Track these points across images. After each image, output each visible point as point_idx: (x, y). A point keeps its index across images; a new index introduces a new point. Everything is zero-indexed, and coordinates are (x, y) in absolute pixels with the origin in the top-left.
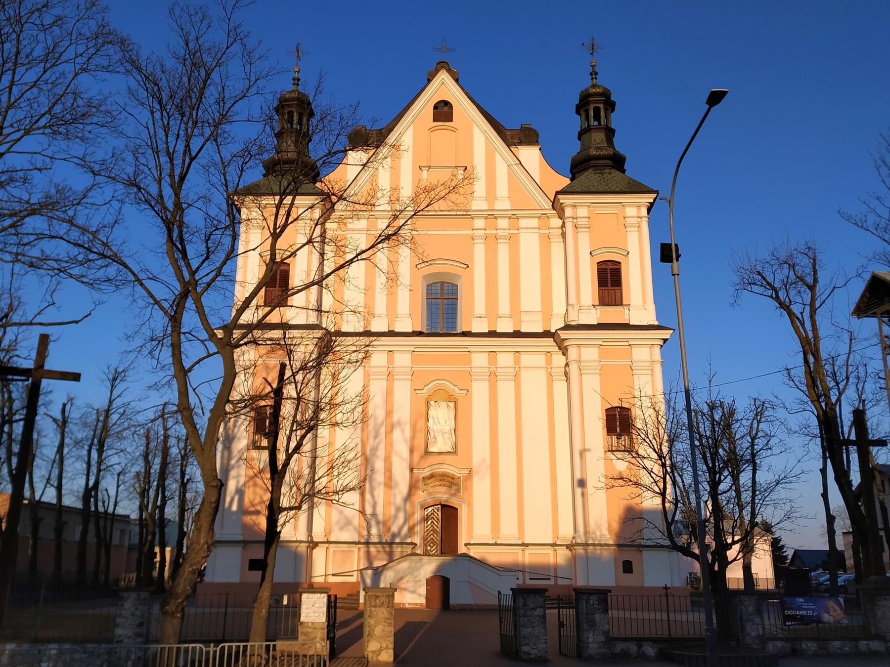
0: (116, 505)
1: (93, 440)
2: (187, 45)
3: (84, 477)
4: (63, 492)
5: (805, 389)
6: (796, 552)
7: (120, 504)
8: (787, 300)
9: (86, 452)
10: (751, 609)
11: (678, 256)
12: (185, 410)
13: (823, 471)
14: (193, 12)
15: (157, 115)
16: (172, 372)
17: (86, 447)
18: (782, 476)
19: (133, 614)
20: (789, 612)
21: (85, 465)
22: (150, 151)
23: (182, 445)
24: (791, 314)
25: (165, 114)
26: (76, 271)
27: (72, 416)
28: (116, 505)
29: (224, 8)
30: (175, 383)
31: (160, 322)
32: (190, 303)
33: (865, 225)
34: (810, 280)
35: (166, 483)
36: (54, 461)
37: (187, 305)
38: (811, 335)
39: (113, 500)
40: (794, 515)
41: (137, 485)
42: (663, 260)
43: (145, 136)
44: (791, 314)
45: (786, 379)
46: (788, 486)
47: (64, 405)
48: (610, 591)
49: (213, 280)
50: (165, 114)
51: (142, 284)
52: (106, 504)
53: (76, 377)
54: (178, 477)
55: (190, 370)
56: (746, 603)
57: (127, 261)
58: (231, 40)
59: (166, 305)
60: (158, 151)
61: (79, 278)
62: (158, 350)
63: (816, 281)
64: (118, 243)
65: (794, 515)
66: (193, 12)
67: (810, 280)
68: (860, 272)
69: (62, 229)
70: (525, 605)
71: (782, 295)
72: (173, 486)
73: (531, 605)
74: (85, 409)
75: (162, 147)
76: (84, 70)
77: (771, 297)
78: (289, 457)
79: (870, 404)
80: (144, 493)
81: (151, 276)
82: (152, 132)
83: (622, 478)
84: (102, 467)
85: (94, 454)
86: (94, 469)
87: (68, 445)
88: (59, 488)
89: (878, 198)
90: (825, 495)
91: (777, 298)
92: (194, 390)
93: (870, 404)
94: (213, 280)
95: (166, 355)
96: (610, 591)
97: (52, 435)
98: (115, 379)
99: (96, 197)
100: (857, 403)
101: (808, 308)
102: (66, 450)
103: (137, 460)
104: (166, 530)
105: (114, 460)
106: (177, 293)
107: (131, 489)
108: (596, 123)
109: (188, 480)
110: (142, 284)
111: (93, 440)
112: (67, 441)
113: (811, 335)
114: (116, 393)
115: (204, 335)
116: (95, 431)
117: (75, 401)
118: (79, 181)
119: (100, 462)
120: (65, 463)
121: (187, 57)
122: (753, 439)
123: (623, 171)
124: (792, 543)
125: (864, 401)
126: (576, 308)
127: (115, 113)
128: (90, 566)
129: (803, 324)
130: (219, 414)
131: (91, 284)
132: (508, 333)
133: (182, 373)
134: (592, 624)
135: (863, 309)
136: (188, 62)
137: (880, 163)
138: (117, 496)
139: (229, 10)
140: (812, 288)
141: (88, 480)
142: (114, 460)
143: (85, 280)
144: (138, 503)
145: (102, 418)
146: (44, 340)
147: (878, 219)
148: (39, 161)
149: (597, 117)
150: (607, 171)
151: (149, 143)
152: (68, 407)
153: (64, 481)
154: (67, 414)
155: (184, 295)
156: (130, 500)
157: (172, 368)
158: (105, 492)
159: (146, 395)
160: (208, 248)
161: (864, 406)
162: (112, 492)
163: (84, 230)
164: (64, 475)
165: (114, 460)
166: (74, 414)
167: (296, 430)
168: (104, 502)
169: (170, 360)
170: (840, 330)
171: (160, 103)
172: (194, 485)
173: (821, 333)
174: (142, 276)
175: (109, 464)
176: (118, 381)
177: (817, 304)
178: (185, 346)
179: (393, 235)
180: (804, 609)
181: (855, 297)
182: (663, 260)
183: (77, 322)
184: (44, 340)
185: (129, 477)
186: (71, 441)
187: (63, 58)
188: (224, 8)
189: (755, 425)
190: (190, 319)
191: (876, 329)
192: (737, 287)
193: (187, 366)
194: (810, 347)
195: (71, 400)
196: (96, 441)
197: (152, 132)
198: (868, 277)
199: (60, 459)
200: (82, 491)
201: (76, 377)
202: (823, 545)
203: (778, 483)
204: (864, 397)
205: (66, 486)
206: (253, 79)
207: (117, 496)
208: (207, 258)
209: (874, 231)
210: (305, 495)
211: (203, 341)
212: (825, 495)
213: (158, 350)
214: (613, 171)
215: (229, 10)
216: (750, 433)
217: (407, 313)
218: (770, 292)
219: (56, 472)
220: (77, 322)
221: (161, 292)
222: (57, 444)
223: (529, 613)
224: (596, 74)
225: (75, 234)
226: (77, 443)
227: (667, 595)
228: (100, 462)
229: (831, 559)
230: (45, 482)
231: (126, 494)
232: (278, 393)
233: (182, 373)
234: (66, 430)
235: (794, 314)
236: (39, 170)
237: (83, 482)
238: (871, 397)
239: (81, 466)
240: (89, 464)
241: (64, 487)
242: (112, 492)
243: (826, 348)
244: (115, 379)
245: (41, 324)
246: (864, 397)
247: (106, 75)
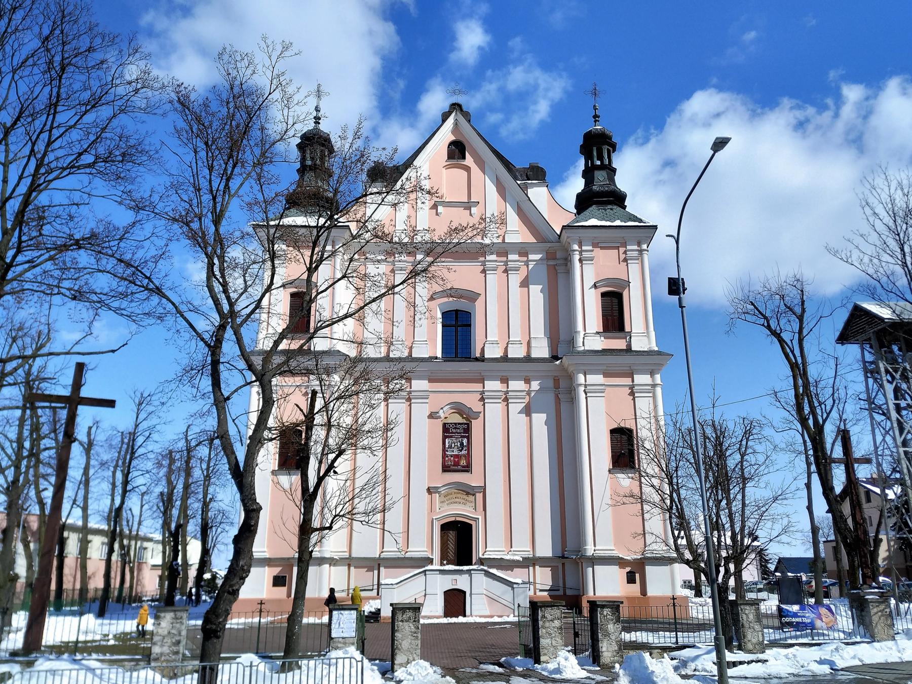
0: (140, 523)
1: (117, 461)
2: (232, 88)
3: (110, 497)
4: (89, 512)
5: (794, 413)
6: (781, 561)
7: (144, 523)
8: (778, 328)
9: (111, 474)
10: (751, 617)
11: (684, 290)
12: (222, 436)
13: (808, 486)
14: (239, 58)
15: (203, 154)
16: (212, 400)
17: (112, 469)
18: (780, 493)
19: (169, 633)
20: (787, 620)
21: (110, 487)
22: (192, 189)
23: (204, 466)
24: (781, 341)
25: (210, 154)
26: (116, 304)
27: (98, 438)
28: (140, 523)
29: (270, 57)
30: (214, 410)
31: (201, 352)
32: (229, 333)
33: (850, 260)
34: (798, 310)
35: (189, 502)
36: (80, 483)
37: (226, 336)
38: (799, 360)
39: (137, 519)
40: (791, 529)
41: (161, 504)
42: (114, 407)
43: (189, 174)
44: (781, 341)
45: (773, 400)
46: (785, 502)
47: (90, 428)
48: (622, 603)
49: (253, 312)
50: (210, 154)
51: (182, 316)
52: (130, 524)
53: (111, 404)
54: (201, 496)
55: (228, 398)
56: (747, 612)
57: (169, 293)
58: (274, 87)
59: (207, 336)
60: (199, 190)
61: (117, 311)
62: (198, 379)
63: (803, 310)
64: (160, 276)
65: (791, 529)
66: (239, 58)
67: (798, 310)
68: (844, 302)
69: (110, 264)
70: (544, 617)
71: (773, 325)
72: (195, 505)
73: (549, 617)
74: (110, 432)
75: (204, 184)
76: (122, 111)
77: (763, 325)
78: (320, 480)
79: (851, 423)
80: (166, 514)
81: (192, 308)
82: (195, 170)
83: (632, 496)
84: (129, 488)
85: (119, 475)
86: (119, 490)
87: (94, 467)
88: (85, 509)
89: (861, 236)
90: (810, 508)
91: (769, 327)
92: (234, 421)
93: (851, 423)
94: (253, 312)
95: (206, 383)
96: (622, 603)
97: (79, 457)
98: (140, 404)
99: (139, 234)
100: (838, 423)
101: (797, 335)
102: (91, 472)
103: (159, 480)
104: (188, 548)
105: (140, 481)
106: (217, 324)
107: (155, 508)
108: (598, 163)
109: (211, 499)
110: (182, 316)
111: (117, 461)
112: (92, 462)
113: (799, 360)
114: (142, 416)
115: (242, 365)
116: (119, 453)
117: (100, 425)
118: (122, 217)
119: (126, 482)
120: (91, 484)
121: (231, 99)
122: (742, 456)
123: (624, 207)
124: (776, 551)
125: (845, 420)
126: (582, 333)
127: (151, 153)
128: (115, 583)
129: (792, 352)
130: (256, 442)
131: (129, 317)
132: (519, 359)
133: (220, 402)
134: (607, 635)
135: (843, 338)
136: (231, 105)
137: (864, 203)
138: (141, 516)
139: (274, 59)
140: (801, 318)
141: (113, 500)
142: (139, 480)
143: (124, 312)
144: (161, 521)
145: (126, 441)
146: (80, 368)
147: (861, 255)
148: (76, 197)
149: (600, 158)
150: (609, 207)
151: (192, 181)
152: (93, 430)
153: (90, 501)
154: (92, 437)
155: (222, 328)
156: (153, 519)
157: (212, 396)
158: (129, 512)
159: (180, 418)
160: (245, 281)
161: (845, 425)
162: (136, 511)
163: (128, 265)
164: (90, 496)
165: (140, 481)
166: (100, 437)
167: (327, 454)
168: (128, 522)
169: (210, 389)
170: (826, 356)
171: (206, 144)
172: (215, 504)
173: (810, 358)
174: (183, 308)
175: (135, 485)
176: (144, 405)
177: (805, 332)
178: (224, 374)
179: (423, 271)
180: (799, 617)
181: (840, 326)
182: (114, 407)
183: (113, 351)
184: (80, 368)
185: (153, 498)
186: (96, 463)
187: (103, 101)
188: (270, 57)
189: (744, 443)
190: (229, 348)
191: (859, 356)
192: (732, 316)
193: (226, 394)
194: (799, 370)
195: (97, 423)
196: (120, 463)
197: (195, 170)
198: (850, 307)
199: (86, 482)
200: (107, 510)
201: (111, 404)
202: (810, 554)
203: (775, 499)
204: (844, 417)
205: (92, 506)
206: (290, 122)
207: (141, 516)
208: (245, 291)
209: (859, 266)
210: (335, 516)
211: (241, 371)
212: (810, 508)
213: (198, 379)
214: (615, 207)
215: (274, 59)
216: (739, 449)
217: (429, 341)
218: (762, 321)
219: (81, 493)
220: (113, 351)
221: (202, 325)
222: (83, 466)
223: (547, 624)
224: (599, 117)
225: (120, 269)
226: (103, 464)
227: (674, 605)
228: (126, 482)
229: (813, 565)
230: (71, 503)
231: (149, 513)
232: (310, 417)
233: (220, 402)
234: (92, 452)
235: (784, 341)
236: (77, 204)
237: (108, 502)
238: (851, 416)
239: (106, 486)
240: (114, 485)
241: (90, 507)
242: (136, 511)
243: (813, 372)
244: (140, 404)
245: (79, 353)
246: (844, 417)
247: (144, 117)
